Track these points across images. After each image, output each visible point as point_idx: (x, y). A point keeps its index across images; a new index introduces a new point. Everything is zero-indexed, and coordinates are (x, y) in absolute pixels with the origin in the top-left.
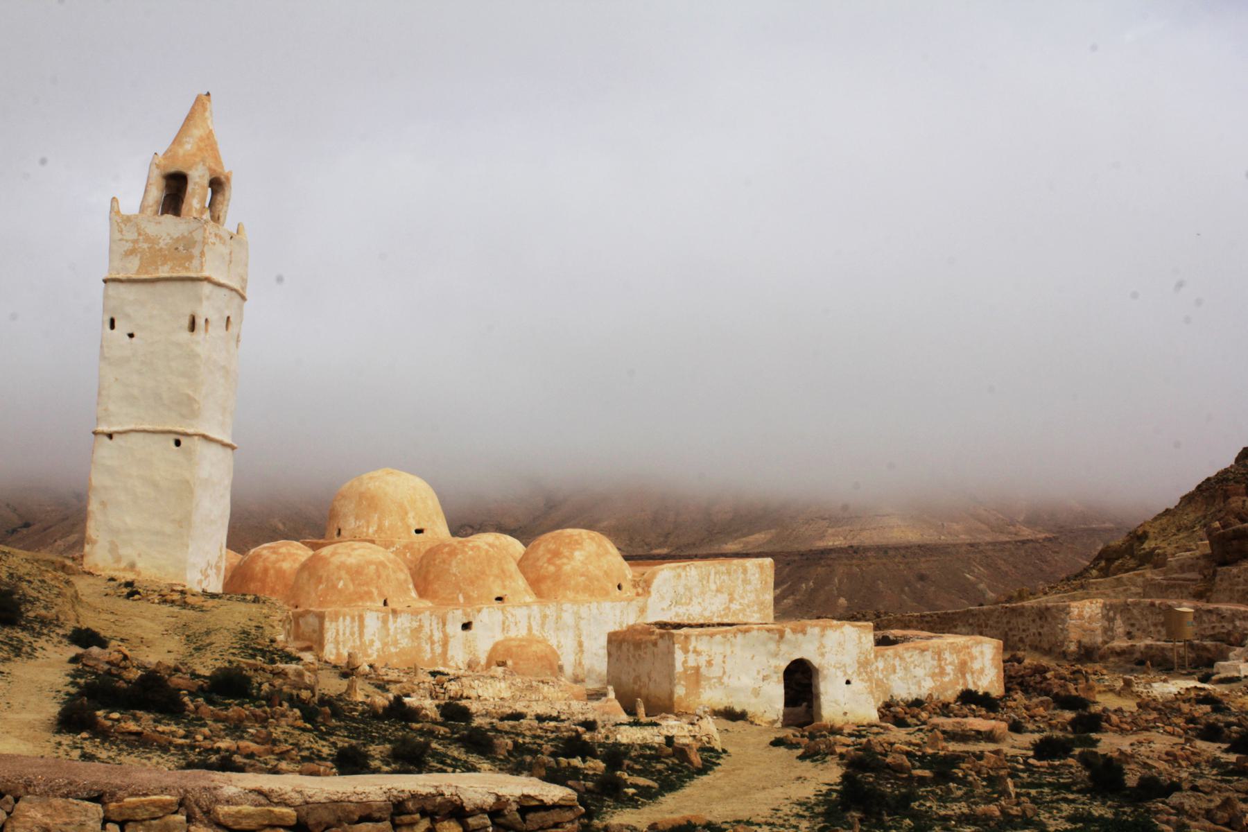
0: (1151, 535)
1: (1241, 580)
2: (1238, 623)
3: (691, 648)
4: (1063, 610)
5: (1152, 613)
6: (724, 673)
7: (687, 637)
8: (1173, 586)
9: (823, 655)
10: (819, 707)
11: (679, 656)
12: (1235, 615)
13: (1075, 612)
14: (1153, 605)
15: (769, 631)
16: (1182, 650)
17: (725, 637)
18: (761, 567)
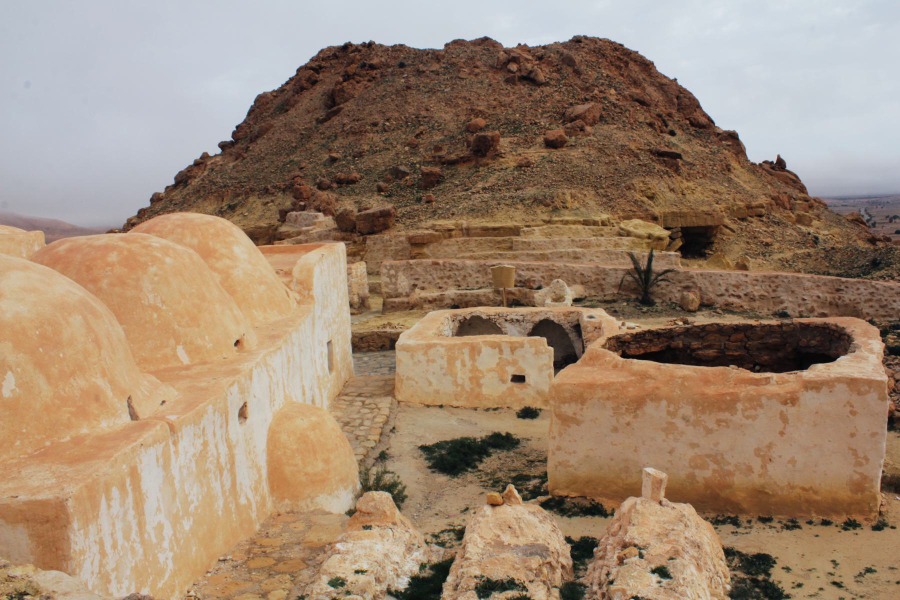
2: (521, 272)
5: (436, 270)
14: (437, 264)
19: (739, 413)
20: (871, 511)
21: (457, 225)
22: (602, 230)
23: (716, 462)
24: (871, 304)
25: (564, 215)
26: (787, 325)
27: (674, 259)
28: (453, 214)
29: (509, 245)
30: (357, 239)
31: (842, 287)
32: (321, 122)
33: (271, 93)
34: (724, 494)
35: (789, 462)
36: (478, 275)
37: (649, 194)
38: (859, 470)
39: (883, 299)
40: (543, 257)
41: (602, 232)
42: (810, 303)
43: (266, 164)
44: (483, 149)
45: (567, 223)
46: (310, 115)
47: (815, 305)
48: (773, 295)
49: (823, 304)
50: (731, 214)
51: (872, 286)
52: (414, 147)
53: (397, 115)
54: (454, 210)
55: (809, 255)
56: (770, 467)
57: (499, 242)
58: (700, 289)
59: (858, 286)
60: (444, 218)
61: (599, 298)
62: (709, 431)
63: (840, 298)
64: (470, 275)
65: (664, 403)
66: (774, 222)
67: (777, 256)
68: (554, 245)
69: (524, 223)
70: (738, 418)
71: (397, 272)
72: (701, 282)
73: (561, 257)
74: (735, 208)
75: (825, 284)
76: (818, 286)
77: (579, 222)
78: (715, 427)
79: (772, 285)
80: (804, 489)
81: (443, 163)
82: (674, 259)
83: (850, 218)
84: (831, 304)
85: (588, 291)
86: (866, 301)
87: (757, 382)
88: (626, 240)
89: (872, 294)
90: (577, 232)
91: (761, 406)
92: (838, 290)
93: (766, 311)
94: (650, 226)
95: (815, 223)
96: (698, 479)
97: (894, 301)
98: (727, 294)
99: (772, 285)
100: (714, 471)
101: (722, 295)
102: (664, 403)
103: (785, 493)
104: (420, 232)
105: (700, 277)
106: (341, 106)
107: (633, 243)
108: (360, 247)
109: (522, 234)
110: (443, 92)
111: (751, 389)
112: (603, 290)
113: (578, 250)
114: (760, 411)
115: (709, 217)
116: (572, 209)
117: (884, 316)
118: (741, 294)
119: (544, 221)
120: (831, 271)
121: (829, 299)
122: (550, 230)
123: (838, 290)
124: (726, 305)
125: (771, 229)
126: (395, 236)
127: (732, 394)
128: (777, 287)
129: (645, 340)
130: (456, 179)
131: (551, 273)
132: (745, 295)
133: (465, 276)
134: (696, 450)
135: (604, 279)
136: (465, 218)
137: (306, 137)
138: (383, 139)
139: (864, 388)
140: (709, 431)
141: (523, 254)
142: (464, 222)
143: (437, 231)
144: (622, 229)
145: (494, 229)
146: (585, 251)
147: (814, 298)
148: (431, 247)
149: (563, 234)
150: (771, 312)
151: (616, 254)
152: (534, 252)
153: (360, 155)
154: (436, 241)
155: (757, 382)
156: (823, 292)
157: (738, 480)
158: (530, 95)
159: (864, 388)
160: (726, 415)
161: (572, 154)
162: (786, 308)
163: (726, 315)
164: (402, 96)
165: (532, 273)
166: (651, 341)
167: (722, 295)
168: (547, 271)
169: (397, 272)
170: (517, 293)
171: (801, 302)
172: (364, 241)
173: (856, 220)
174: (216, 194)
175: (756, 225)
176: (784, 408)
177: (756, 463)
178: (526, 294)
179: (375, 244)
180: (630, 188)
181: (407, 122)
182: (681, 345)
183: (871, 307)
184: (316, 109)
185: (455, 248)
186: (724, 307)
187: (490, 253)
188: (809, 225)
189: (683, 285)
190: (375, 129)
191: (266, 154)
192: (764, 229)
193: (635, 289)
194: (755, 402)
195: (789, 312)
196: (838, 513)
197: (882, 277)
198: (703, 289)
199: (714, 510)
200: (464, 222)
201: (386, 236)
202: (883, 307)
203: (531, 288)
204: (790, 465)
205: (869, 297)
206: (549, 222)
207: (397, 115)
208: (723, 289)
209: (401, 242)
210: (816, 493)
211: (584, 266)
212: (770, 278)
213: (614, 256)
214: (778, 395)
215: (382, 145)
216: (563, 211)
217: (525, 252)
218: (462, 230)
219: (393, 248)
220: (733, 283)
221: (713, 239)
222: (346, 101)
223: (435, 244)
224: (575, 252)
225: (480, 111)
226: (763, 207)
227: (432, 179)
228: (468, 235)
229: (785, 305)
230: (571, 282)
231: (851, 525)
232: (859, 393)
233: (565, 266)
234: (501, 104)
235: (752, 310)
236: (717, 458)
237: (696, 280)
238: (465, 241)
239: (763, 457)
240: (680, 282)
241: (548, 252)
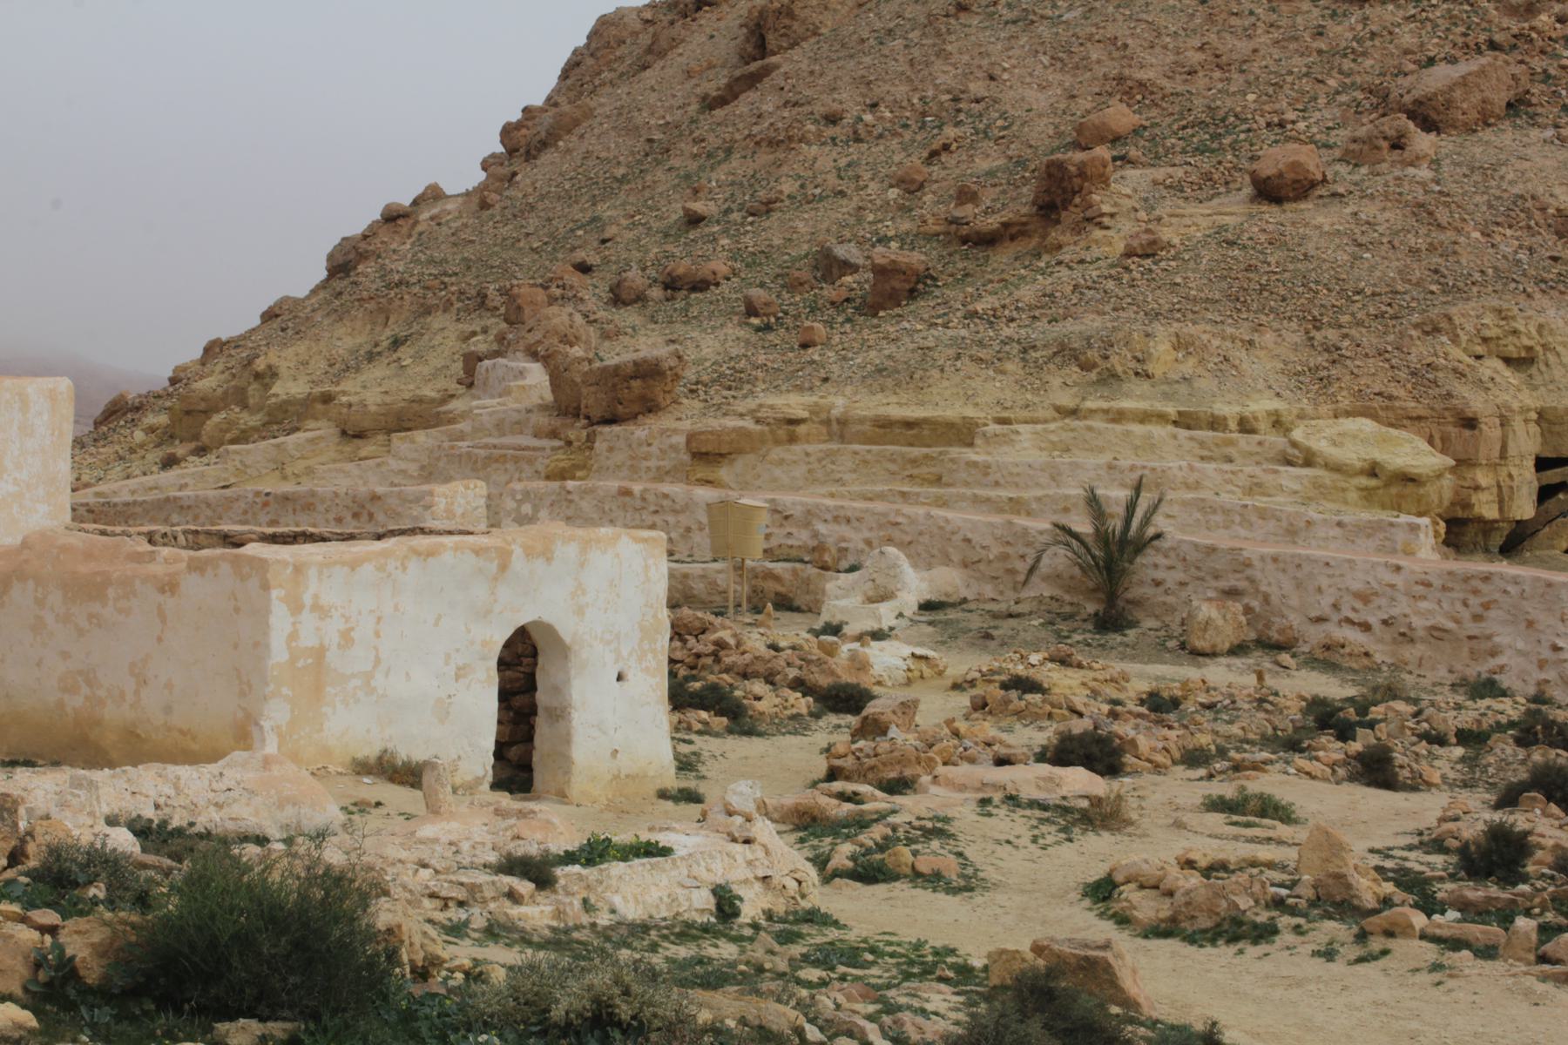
0: (283, 371)
1: (654, 449)
2: (822, 528)
3: (307, 599)
4: (417, 500)
5: (624, 507)
6: (378, 661)
7: (299, 569)
8: (502, 459)
9: (580, 611)
10: (567, 740)
11: (280, 619)
12: (810, 514)
13: (441, 504)
14: (626, 493)
15: (478, 552)
16: (721, 581)
17: (381, 568)
18: (52, 396)
22: (1231, 443)
23: (89, 683)
25: (1127, 396)
28: (826, 380)
30: (572, 435)
32: (711, 103)
33: (639, 11)
37: (1512, 351)
41: (1232, 451)
43: (533, 223)
44: (1060, 197)
45: (1119, 417)
46: (689, 85)
48: (1473, 629)
52: (912, 187)
53: (901, 90)
57: (914, 462)
65: (31, 584)
71: (536, 509)
77: (1161, 418)
79: (1474, 601)
80: (182, 732)
81: (965, 240)
88: (1291, 477)
90: (1150, 446)
93: (1442, 671)
96: (69, 710)
98: (1335, 617)
100: (86, 698)
101: (1320, 620)
102: (31, 584)
104: (731, 423)
105: (1270, 566)
106: (774, 59)
107: (1317, 485)
108: (578, 458)
109: (978, 441)
110: (1056, 21)
118: (1373, 620)
119: (1058, 409)
122: (1064, 435)
124: (1327, 648)
126: (663, 432)
128: (1486, 606)
130: (971, 284)
132: (1385, 622)
133: (688, 530)
137: (657, 151)
138: (843, 162)
140: (81, 632)
141: (963, 498)
143: (758, 422)
144: (1294, 444)
145: (909, 424)
148: (740, 463)
150: (1451, 678)
151: (1227, 512)
152: (992, 493)
153: (767, 207)
154: (753, 450)
158: (1320, 33)
161: (1320, 219)
164: (939, 34)
165: (844, 530)
167: (1320, 620)
168: (881, 526)
169: (536, 509)
170: (787, 576)
171: (1547, 654)
172: (591, 439)
174: (371, 306)
178: (807, 581)
179: (611, 449)
180: (1437, 330)
181: (924, 114)
184: (711, 66)
185: (799, 471)
186: (1319, 654)
187: (879, 488)
189: (1223, 584)
190: (830, 131)
191: (542, 197)
195: (1505, 681)
198: (1274, 599)
201: (639, 431)
203: (825, 568)
206: (1073, 413)
207: (901, 90)
208: (1326, 602)
209: (673, 447)
213: (1218, 518)
214: (155, 577)
215: (832, 180)
217: (968, 492)
219: (653, 463)
220: (1357, 586)
222: (792, 46)
223: (750, 458)
225: (1141, 84)
227: (897, 284)
228: (842, 439)
230: (923, 561)
233: (929, 516)
234: (1220, 63)
237: (1258, 575)
238: (829, 454)
240: (1216, 578)
241: (1026, 495)
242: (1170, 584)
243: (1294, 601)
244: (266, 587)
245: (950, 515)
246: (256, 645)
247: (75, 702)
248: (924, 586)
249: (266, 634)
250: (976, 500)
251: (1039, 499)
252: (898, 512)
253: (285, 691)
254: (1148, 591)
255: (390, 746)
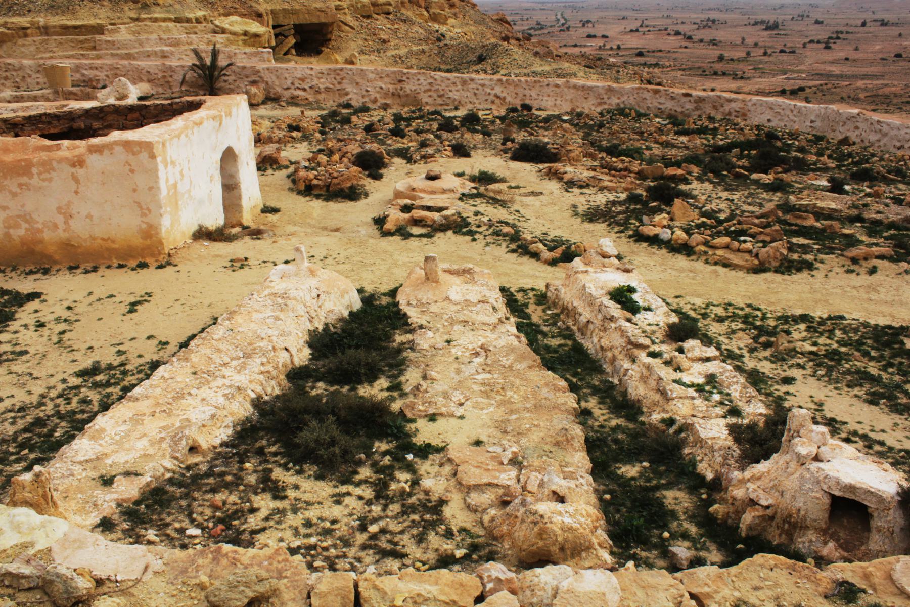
2: (85, 72)
19: (36, 176)
20: (160, 254)
21: (32, 23)
22: (195, 27)
23: (27, 221)
24: (430, 93)
25: (154, 12)
26: (177, 103)
27: (266, 56)
28: (29, 11)
29: (92, 44)
31: (404, 78)
34: (38, 248)
35: (87, 217)
36: (38, 75)
38: (145, 219)
39: (440, 88)
40: (129, 56)
41: (196, 30)
42: (374, 94)
45: (156, 20)
47: (378, 96)
48: (338, 87)
49: (386, 95)
50: (355, 11)
51: (431, 77)
54: (31, 5)
55: (423, 51)
56: (71, 222)
57: (81, 42)
58: (267, 83)
59: (419, 77)
60: (19, 15)
61: (166, 96)
62: (14, 195)
63: (401, 89)
64: (30, 76)
66: (401, 20)
67: (389, 53)
68: (141, 44)
69: (108, 21)
70: (35, 181)
72: (268, 77)
73: (148, 56)
74: (359, 5)
75: (388, 76)
76: (381, 78)
77: (170, 20)
78: (18, 190)
79: (338, 77)
80: (103, 239)
82: (266, 56)
83: (495, 18)
84: (393, 94)
85: (155, 89)
86: (425, 91)
87: (48, 149)
89: (430, 84)
90: (168, 30)
91: (53, 170)
92: (400, 81)
93: (331, 102)
94: (246, 23)
95: (451, 21)
96: (15, 237)
97: (451, 91)
99: (338, 77)
100: (27, 229)
101: (288, 89)
103: (88, 244)
105: (267, 72)
107: (228, 40)
109: (106, 32)
111: (44, 155)
112: (170, 87)
113: (165, 48)
114: (54, 174)
115: (322, 14)
116: (165, 6)
117: (442, 105)
118: (306, 87)
119: (131, 18)
120: (442, 67)
121: (391, 90)
122: (137, 28)
123: (400, 81)
124: (292, 98)
125: (396, 26)
127: (25, 160)
128: (342, 79)
129: (43, 123)
131: (116, 71)
132: (311, 87)
134: (7, 212)
135: (171, 76)
136: (42, 15)
139: (136, 149)
140: (14, 195)
141: (107, 54)
142: (41, 20)
143: (8, 29)
144: (217, 26)
145: (75, 27)
146: (173, 49)
147: (377, 89)
149: (152, 33)
152: (119, 52)
154: (10, 41)
155: (48, 149)
156: (385, 83)
157: (47, 235)
159: (136, 149)
160: (24, 179)
162: (351, 99)
163: (290, 108)
165: (97, 73)
166: (49, 123)
167: (288, 89)
168: (111, 70)
170: (79, 93)
171: (364, 93)
173: (501, 20)
175: (381, 22)
176: (74, 170)
177: (59, 220)
182: (83, 126)
183: (430, 96)
185: (33, 48)
186: (290, 100)
187: (71, 53)
188: (444, 23)
189: (250, 79)
192: (389, 26)
193: (203, 85)
194: (47, 166)
196: (134, 257)
197: (477, 72)
198: (270, 83)
199: (34, 263)
200: (41, 20)
202: (440, 96)
203: (94, 88)
204: (88, 220)
205: (428, 87)
206: (137, 20)
208: (289, 82)
210: (113, 242)
211: (151, 64)
212: (335, 71)
214: (67, 158)
216: (154, 8)
217: (109, 52)
218: (39, 28)
220: (299, 76)
221: (329, 36)
223: (9, 44)
224: (163, 51)
226: (390, 4)
228: (47, 34)
229: (350, 96)
231: (143, 265)
232: (134, 154)
233: (130, 64)
235: (317, 102)
236: (26, 218)
237: (263, 75)
238: (44, 41)
239: (64, 214)
241: (133, 51)
242: (230, 81)
243: (277, 83)
244: (153, 157)
245: (139, 63)
246: (151, 188)
247: (19, 233)
248: (138, 91)
249: (157, 182)
250: (113, 55)
251: (137, 53)
252: (117, 64)
253: (168, 209)
254: (223, 84)
255: (200, 222)
